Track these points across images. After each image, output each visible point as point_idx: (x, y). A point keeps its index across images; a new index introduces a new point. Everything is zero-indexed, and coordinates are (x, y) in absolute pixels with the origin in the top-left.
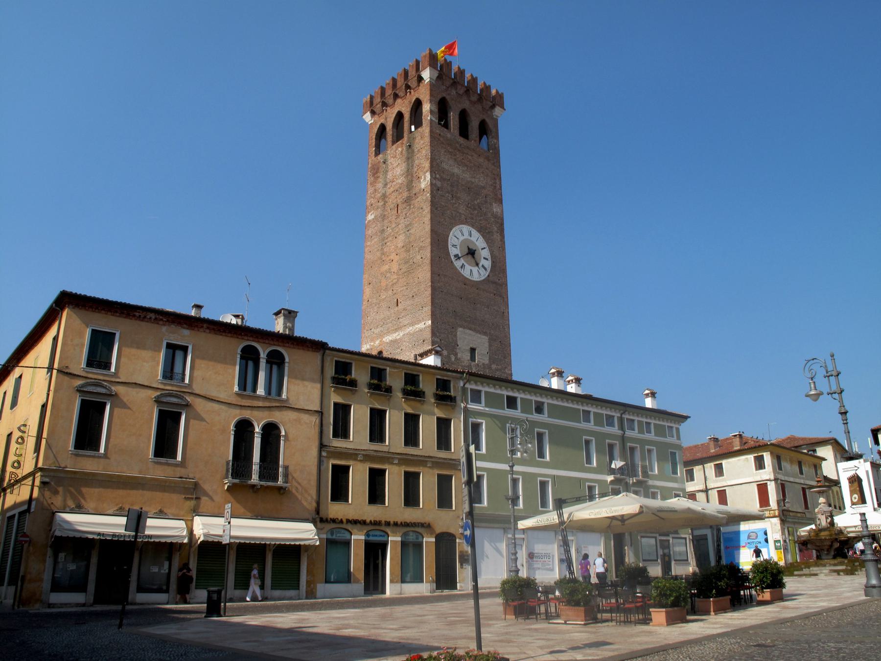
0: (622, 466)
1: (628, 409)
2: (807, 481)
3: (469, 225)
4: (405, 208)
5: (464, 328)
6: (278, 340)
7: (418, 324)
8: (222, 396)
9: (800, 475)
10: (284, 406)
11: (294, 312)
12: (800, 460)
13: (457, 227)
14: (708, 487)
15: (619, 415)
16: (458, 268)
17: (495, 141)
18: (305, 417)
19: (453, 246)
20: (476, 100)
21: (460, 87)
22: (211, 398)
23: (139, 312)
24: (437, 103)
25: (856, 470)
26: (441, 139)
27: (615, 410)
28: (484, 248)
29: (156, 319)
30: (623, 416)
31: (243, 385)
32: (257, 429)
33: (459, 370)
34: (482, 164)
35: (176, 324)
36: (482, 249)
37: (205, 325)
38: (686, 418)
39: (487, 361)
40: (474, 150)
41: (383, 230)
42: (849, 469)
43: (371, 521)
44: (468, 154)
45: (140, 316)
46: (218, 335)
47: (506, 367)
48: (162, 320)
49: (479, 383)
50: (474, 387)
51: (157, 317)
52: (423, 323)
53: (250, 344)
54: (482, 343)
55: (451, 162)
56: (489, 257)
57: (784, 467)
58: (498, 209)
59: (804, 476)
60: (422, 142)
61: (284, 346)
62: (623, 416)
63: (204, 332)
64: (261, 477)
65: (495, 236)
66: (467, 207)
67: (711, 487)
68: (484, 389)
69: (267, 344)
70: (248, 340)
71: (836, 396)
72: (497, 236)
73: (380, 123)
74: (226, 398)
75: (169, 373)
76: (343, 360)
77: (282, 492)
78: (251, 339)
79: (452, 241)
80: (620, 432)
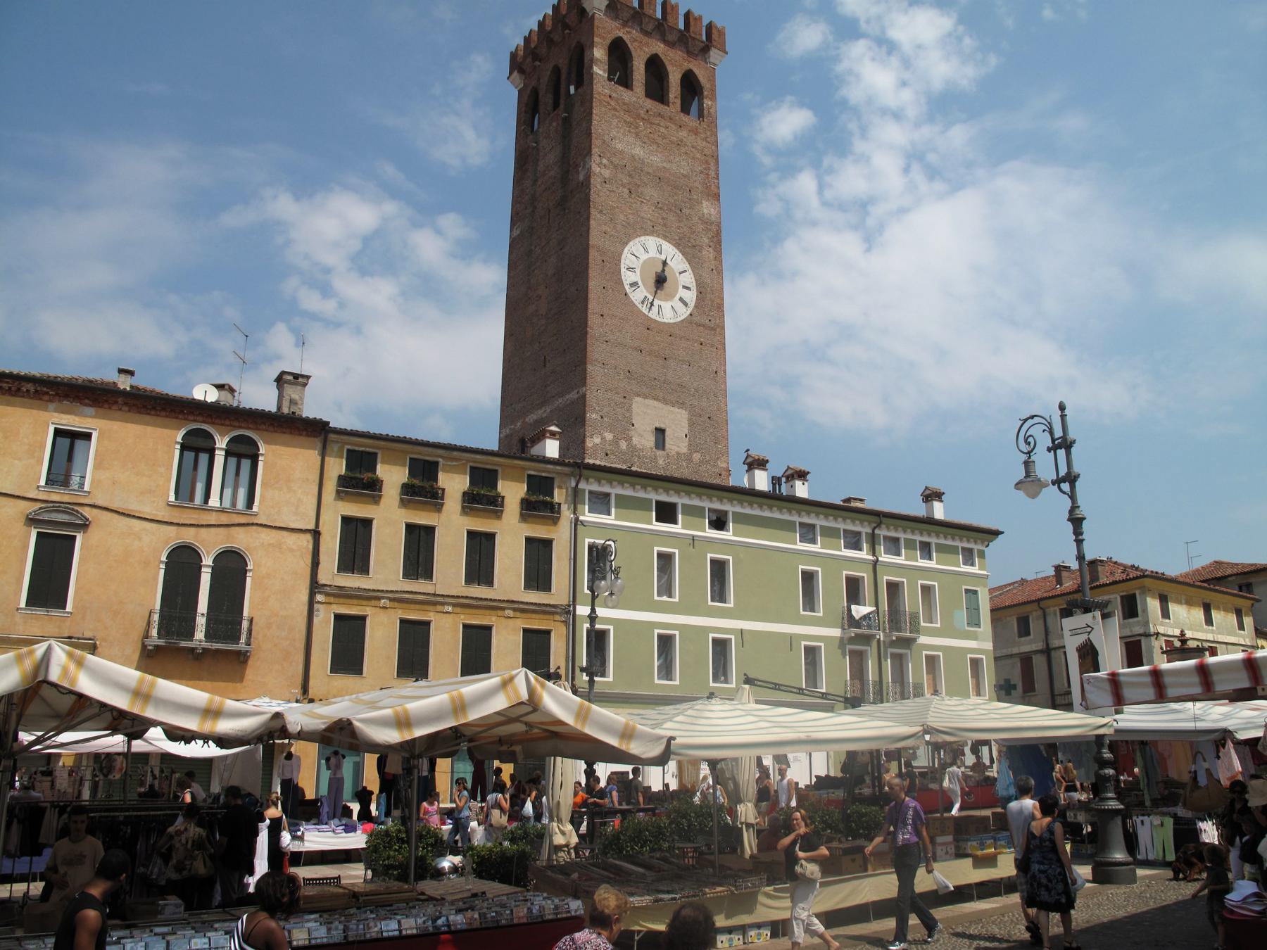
0: (870, 613)
1: (884, 520)
2: (1219, 636)
3: (658, 236)
4: (558, 215)
5: (645, 397)
7: (569, 393)
8: (147, 510)
9: (1205, 627)
11: (303, 376)
12: (1208, 601)
13: (637, 240)
14: (1051, 646)
16: (636, 303)
17: (710, 103)
18: (291, 540)
19: (627, 269)
20: (676, 39)
21: (647, 20)
22: (127, 512)
23: (7, 383)
24: (607, 48)
25: (1090, 633)
26: (613, 103)
27: (862, 522)
28: (685, 271)
29: (37, 391)
30: (877, 531)
31: (184, 490)
32: (208, 561)
33: (567, 461)
35: (71, 400)
36: (680, 273)
37: (120, 400)
38: (996, 533)
39: (684, 450)
40: (671, 119)
41: (531, 251)
42: (1080, 631)
44: (659, 125)
45: (10, 388)
46: (142, 413)
47: (718, 458)
48: (47, 393)
49: (591, 480)
50: (595, 487)
51: (39, 388)
52: (576, 391)
53: (199, 427)
54: (677, 422)
55: (631, 139)
56: (693, 285)
57: (1173, 614)
59: (1214, 628)
60: (582, 110)
61: (257, 429)
62: (877, 531)
63: (120, 410)
64: (209, 635)
65: (704, 252)
66: (656, 207)
67: (1054, 646)
68: (615, 490)
69: (228, 426)
70: (195, 421)
71: (1066, 486)
72: (708, 254)
73: (531, 87)
74: (154, 512)
75: (60, 475)
76: (361, 449)
77: (242, 658)
78: (200, 418)
79: (627, 262)
80: (871, 557)
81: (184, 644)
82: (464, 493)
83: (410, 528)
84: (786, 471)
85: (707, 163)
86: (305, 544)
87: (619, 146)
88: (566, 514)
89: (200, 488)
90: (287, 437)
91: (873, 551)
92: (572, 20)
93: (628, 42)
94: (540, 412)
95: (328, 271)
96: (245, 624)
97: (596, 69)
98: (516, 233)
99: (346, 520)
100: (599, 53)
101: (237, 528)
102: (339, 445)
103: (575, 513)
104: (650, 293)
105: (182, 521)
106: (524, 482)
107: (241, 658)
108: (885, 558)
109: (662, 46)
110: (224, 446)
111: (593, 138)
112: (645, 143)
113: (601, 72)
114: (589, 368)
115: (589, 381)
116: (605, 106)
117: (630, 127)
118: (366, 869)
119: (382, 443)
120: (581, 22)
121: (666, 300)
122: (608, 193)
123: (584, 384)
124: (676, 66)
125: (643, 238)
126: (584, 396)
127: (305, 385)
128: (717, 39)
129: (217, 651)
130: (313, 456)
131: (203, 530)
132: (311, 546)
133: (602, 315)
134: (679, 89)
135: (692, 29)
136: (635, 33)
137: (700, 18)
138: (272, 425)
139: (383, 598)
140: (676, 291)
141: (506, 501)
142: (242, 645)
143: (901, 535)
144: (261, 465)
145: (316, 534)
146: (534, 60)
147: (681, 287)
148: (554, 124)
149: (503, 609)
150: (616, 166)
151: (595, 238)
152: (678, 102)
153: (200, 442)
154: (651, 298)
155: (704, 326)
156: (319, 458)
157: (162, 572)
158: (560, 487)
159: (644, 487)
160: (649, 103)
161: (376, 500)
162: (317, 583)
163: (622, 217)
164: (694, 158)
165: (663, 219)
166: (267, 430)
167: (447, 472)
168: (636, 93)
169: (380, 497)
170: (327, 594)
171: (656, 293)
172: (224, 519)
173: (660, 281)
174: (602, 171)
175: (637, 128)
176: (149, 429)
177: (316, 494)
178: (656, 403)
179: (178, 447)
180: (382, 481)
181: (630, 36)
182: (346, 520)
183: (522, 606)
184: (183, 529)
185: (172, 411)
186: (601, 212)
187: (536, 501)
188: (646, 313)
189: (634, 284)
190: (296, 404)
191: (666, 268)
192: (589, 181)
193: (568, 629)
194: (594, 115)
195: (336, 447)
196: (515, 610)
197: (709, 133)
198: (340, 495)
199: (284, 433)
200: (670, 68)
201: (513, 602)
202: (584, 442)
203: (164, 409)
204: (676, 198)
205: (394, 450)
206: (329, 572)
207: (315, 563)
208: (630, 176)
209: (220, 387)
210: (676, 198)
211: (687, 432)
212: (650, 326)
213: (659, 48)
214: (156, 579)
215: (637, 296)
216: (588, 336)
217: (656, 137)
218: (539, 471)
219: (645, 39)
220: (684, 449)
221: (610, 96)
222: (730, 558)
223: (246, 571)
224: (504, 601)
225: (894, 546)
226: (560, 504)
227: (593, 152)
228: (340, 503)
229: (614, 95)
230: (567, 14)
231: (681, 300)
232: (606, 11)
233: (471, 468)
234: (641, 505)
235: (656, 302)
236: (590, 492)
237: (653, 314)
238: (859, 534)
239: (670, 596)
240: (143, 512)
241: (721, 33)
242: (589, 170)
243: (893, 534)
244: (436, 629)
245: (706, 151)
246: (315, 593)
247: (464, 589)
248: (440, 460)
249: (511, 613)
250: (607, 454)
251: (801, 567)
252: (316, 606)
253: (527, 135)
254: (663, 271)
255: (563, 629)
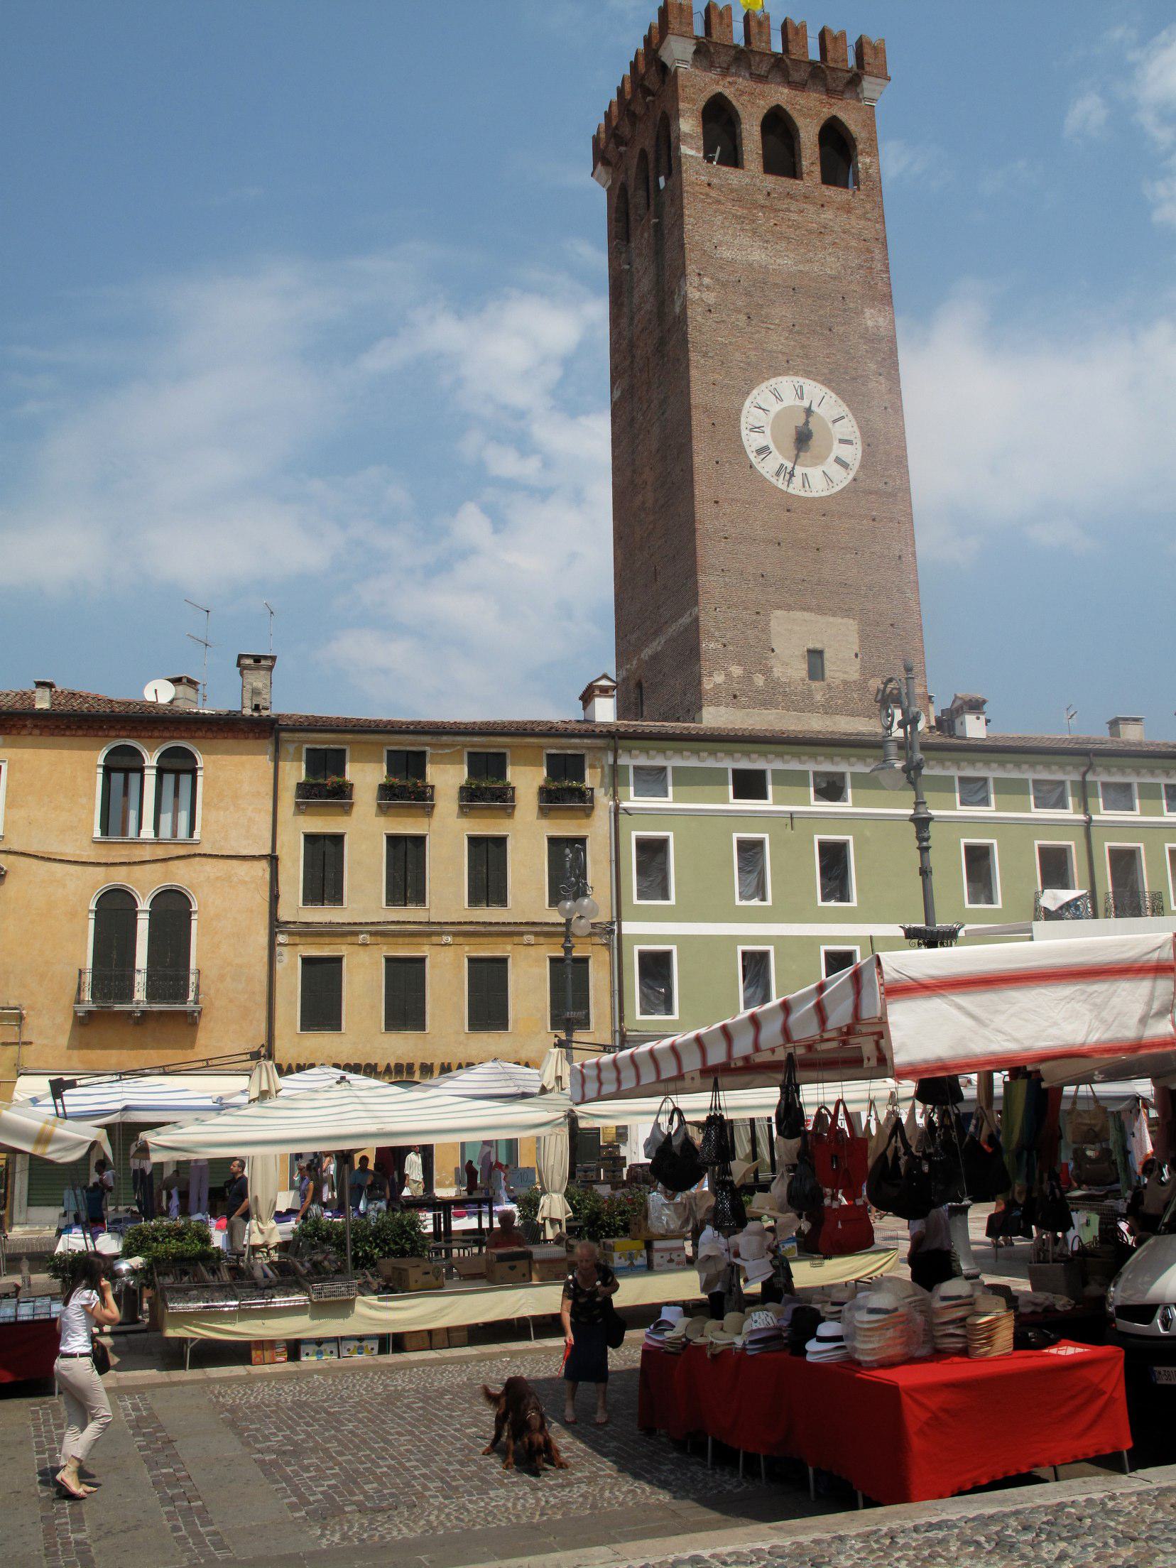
0: (1076, 899)
1: (1096, 760)
3: (796, 374)
5: (789, 608)
6: (177, 729)
8: (70, 851)
10: (195, 855)
11: (266, 657)
13: (763, 386)
15: (1078, 778)
16: (768, 476)
17: (868, 160)
19: (751, 430)
22: (46, 856)
24: (699, 115)
28: (843, 418)
30: (1089, 778)
32: (144, 905)
34: (831, 224)
36: (835, 421)
39: (855, 676)
40: (806, 197)
41: (633, 419)
43: (388, 1066)
50: (643, 761)
55: (745, 240)
58: (881, 319)
63: (30, 734)
64: (152, 995)
65: (872, 385)
66: (791, 331)
68: (672, 762)
69: (157, 738)
70: (118, 737)
72: (878, 385)
74: (78, 852)
77: (190, 1020)
78: (124, 733)
80: (1081, 817)
81: (118, 1007)
82: (462, 789)
83: (393, 840)
84: (954, 702)
85: (869, 251)
86: (261, 874)
87: (727, 254)
88: (603, 801)
89: (133, 815)
90: (231, 743)
91: (1085, 807)
92: (652, 81)
93: (731, 97)
94: (655, 644)
95: (520, 415)
96: (192, 978)
97: (685, 150)
98: (617, 394)
99: (311, 839)
100: (689, 125)
101: (176, 862)
102: (296, 745)
103: (615, 800)
104: (788, 458)
105: (111, 860)
106: (541, 766)
107: (190, 1021)
108: (1103, 815)
109: (786, 91)
110: (155, 764)
111: (687, 251)
112: (767, 242)
113: (692, 153)
114: (702, 578)
115: (702, 599)
116: (703, 201)
117: (743, 222)
118: (74, 1189)
119: (349, 737)
120: (663, 82)
121: (814, 465)
122: (714, 325)
123: (696, 603)
124: (810, 116)
125: (773, 381)
126: (697, 620)
127: (270, 668)
128: (871, 61)
129: (161, 1013)
130: (264, 762)
131: (136, 868)
132: (267, 876)
133: (716, 502)
134: (817, 149)
135: (830, 55)
136: (743, 82)
137: (843, 35)
138: (209, 730)
139: (362, 932)
140: (829, 449)
141: (518, 793)
142: (189, 1006)
143: (1134, 780)
144: (200, 780)
145: (273, 860)
146: (618, 145)
147: (836, 443)
148: (646, 235)
149: (521, 934)
150: (724, 285)
151: (699, 394)
152: (817, 169)
153: (126, 762)
154: (789, 465)
155: (876, 493)
156: (271, 765)
157: (92, 923)
158: (593, 767)
159: (713, 753)
160: (771, 182)
161: (347, 809)
162: (277, 920)
163: (738, 356)
164: (847, 248)
165: (803, 347)
166: (204, 738)
167: (437, 763)
168: (749, 170)
169: (352, 805)
170: (290, 934)
171: (797, 456)
172: (161, 852)
173: (803, 439)
174: (704, 296)
175: (754, 221)
176: (66, 753)
177: (271, 809)
178: (807, 615)
179: (100, 770)
180: (352, 785)
181: (736, 89)
182: (311, 839)
183: (546, 929)
184: (112, 869)
185: (90, 728)
186: (705, 355)
187: (558, 789)
188: (784, 488)
189: (763, 451)
190: (259, 694)
191: (810, 419)
192: (686, 314)
193: (611, 954)
194: (686, 218)
195: (291, 748)
196: (536, 934)
197: (868, 206)
198: (300, 808)
199: (225, 738)
200: (800, 122)
201: (534, 924)
202: (700, 683)
203: (80, 727)
204: (821, 312)
205: (372, 743)
206: (293, 906)
207: (274, 898)
208: (748, 294)
209: (176, 681)
210: (821, 312)
211: (857, 650)
212: (790, 505)
213: (780, 95)
214: (85, 931)
215: (767, 468)
216: (698, 534)
217: (784, 229)
218: (562, 748)
219: (759, 87)
220: (854, 674)
221: (709, 185)
222: (850, 838)
223: (190, 914)
224: (521, 923)
225: (1120, 796)
226: (592, 789)
227: (688, 271)
228: (302, 818)
229: (715, 181)
230: (646, 72)
231: (838, 460)
232: (694, 60)
233: (470, 754)
234: (711, 778)
235: (799, 471)
236: (636, 768)
237: (795, 488)
238: (1062, 783)
239: (764, 899)
240: (66, 854)
241: (879, 50)
242: (685, 296)
243: (1118, 779)
244: (433, 967)
245: (867, 234)
246: (276, 933)
247: (465, 913)
248: (427, 748)
249: (531, 939)
250: (735, 697)
251: (963, 841)
252: (278, 949)
253: (621, 253)
254: (807, 423)
255: (604, 955)
